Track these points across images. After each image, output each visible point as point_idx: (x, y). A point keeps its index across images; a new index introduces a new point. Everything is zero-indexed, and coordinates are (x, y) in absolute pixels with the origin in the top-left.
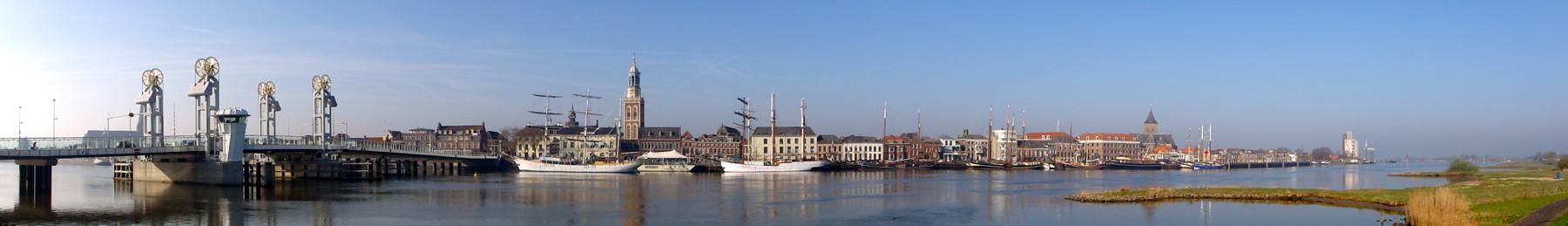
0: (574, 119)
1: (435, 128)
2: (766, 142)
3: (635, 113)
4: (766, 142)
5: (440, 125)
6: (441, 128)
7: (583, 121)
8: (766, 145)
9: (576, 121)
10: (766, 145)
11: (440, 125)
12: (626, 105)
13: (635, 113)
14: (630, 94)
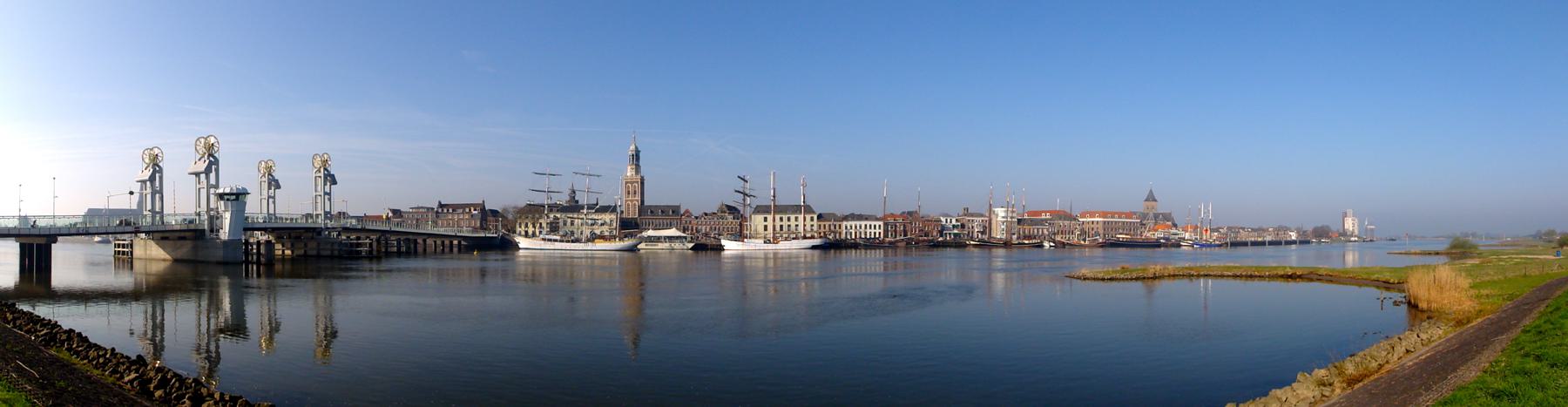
0: (574, 197)
1: (435, 206)
2: (766, 219)
3: (635, 191)
4: (766, 219)
5: (440, 202)
6: (441, 206)
7: (583, 199)
8: (766, 223)
9: (576, 199)
10: (766, 223)
11: (440, 202)
12: (626, 183)
13: (635, 191)
14: (630, 172)
